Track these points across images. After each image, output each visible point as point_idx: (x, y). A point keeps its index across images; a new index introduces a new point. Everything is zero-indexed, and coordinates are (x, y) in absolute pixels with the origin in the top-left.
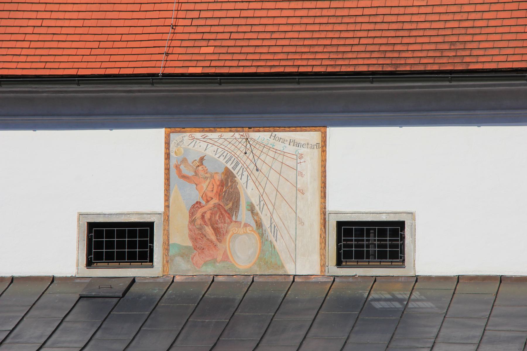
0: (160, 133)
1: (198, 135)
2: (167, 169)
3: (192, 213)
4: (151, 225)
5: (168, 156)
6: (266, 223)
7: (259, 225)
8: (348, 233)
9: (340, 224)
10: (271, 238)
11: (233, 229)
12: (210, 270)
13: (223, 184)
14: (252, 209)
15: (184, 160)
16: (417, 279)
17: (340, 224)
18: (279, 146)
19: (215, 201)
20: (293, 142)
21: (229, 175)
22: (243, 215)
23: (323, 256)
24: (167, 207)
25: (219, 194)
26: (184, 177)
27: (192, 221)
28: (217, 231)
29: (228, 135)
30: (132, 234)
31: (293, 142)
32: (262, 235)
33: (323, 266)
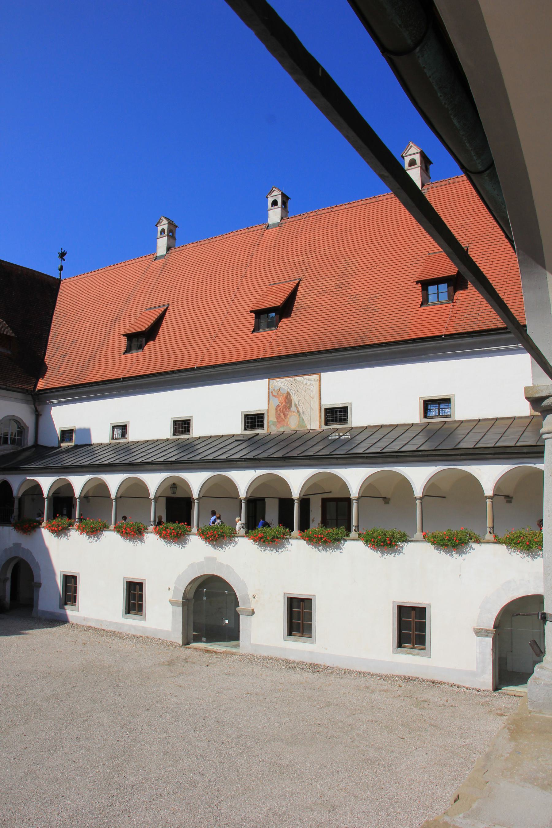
0: (266, 381)
1: (278, 380)
2: (269, 393)
3: (276, 409)
4: (263, 414)
5: (269, 389)
6: (301, 411)
7: (298, 411)
8: (329, 412)
9: (326, 409)
10: (303, 416)
11: (290, 414)
12: (282, 430)
13: (286, 397)
14: (296, 406)
15: (274, 390)
16: (352, 428)
17: (326, 409)
18: (305, 381)
19: (284, 404)
20: (310, 380)
21: (288, 394)
22: (293, 408)
23: (320, 422)
24: (269, 407)
25: (285, 401)
26: (274, 396)
27: (277, 412)
28: (284, 415)
29: (288, 379)
30: (341, 412)
31: (310, 380)
32: (299, 415)
33: (320, 425)
